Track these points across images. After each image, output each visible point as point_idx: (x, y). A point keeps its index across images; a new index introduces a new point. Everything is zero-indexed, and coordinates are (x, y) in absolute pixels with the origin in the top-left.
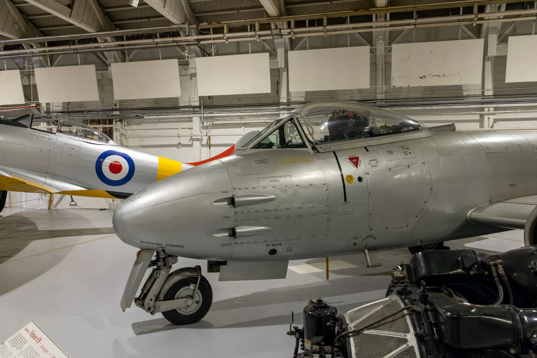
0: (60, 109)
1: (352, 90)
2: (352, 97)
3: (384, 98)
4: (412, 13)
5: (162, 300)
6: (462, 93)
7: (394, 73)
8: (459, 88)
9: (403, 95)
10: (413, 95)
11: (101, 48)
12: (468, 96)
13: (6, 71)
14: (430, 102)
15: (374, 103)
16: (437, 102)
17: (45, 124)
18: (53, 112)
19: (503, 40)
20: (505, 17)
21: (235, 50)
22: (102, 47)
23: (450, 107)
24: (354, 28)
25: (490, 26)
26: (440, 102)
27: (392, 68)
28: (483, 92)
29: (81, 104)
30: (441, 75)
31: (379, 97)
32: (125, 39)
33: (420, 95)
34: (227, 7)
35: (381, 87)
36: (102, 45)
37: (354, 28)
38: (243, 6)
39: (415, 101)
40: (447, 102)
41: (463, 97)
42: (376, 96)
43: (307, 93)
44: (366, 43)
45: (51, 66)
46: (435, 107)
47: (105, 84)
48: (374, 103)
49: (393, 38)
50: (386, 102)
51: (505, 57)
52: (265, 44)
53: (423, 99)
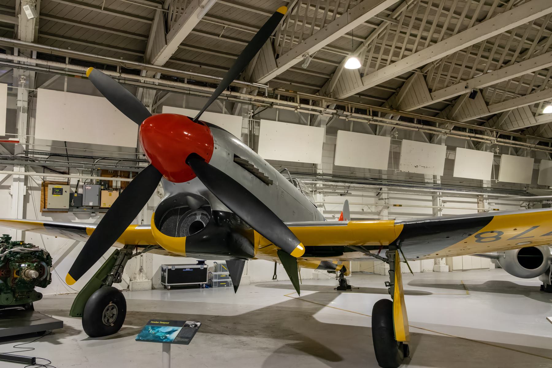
0: (48, 149)
4: (510, 136)
7: (402, 161)
8: (422, 176)
10: (368, 175)
11: (140, 82)
13: (465, 149)
17: (23, 169)
18: (33, 153)
20: (397, 124)
21: (298, 122)
22: (142, 81)
24: (469, 136)
29: (87, 146)
34: (115, 45)
36: (142, 79)
38: (295, 80)
40: (410, 185)
43: (54, 142)
44: (427, 140)
45: (310, 125)
46: (415, 189)
47: (395, 157)
49: (40, 80)
52: (302, 118)
53: (405, 182)
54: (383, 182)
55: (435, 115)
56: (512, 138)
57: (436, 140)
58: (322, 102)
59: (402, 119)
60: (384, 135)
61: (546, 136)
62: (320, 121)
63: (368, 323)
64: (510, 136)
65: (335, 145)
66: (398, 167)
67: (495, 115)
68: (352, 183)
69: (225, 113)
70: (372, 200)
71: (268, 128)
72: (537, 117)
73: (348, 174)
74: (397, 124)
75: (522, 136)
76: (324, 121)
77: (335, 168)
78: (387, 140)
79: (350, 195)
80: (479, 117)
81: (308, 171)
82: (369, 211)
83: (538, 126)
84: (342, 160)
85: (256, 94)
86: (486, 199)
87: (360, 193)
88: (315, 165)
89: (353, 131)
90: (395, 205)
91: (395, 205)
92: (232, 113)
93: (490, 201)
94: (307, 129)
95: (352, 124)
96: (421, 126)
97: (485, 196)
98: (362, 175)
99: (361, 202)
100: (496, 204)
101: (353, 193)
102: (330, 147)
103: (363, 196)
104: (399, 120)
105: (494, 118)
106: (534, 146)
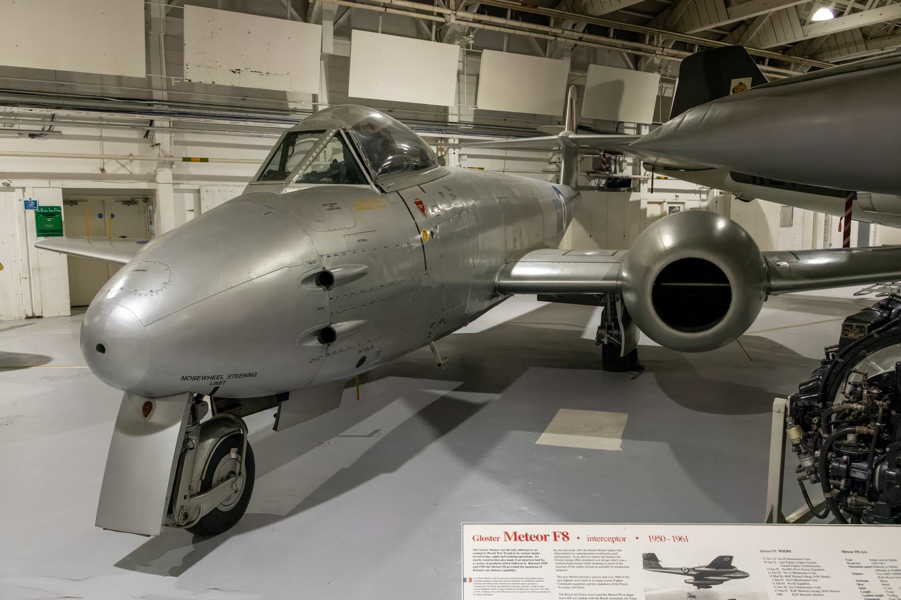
1: (101, 76)
2: (102, 89)
3: (166, 98)
4: (765, 58)
5: (198, 494)
6: (287, 105)
7: (189, 57)
8: (282, 96)
9: (197, 98)
12: (295, 111)
13: (379, 35)
14: (244, 114)
15: (149, 105)
16: (254, 115)
19: (343, 32)
20: (475, 21)
23: (272, 125)
24: (531, 30)
25: (324, 7)
26: (258, 115)
27: (186, 48)
28: (315, 107)
30: (264, 72)
31: (157, 95)
32: (611, 35)
33: (224, 100)
35: (159, 79)
37: (531, 30)
39: (217, 110)
40: (237, 114)
41: (287, 111)
42: (151, 93)
43: (595, 120)
46: (251, 124)
48: (149, 105)
50: (170, 106)
51: (346, 61)
53: (231, 107)
54: (155, 108)
55: (646, 23)
56: (767, 61)
57: (643, 65)
58: (658, 37)
59: (591, 29)
60: (451, 41)
61: (590, 11)
62: (321, 10)
63: (601, 358)
64: (765, 58)
65: (478, 76)
66: (181, 73)
67: (743, 22)
68: (59, 107)
69: (293, 18)
70: (134, 149)
71: (366, 46)
72: (806, 27)
73: (49, 86)
74: (580, 39)
75: (785, 58)
76: (331, 12)
77: (478, 113)
78: (565, 64)
79: (59, 135)
80: (714, 26)
81: (435, 118)
82: (123, 171)
83: (812, 40)
84: (491, 99)
85: (475, 10)
86: (454, 146)
87: (95, 132)
88: (446, 109)
89: (508, 51)
90: (186, 159)
91: (186, 159)
92: (637, 68)
93: (464, 151)
94: (432, 46)
95: (506, 39)
96: (620, 42)
97: (451, 141)
98: (95, 90)
99: (97, 152)
100: (469, 156)
101: (66, 130)
102: (469, 76)
103: (101, 138)
104: (584, 32)
105: (742, 28)
106: (577, 35)
